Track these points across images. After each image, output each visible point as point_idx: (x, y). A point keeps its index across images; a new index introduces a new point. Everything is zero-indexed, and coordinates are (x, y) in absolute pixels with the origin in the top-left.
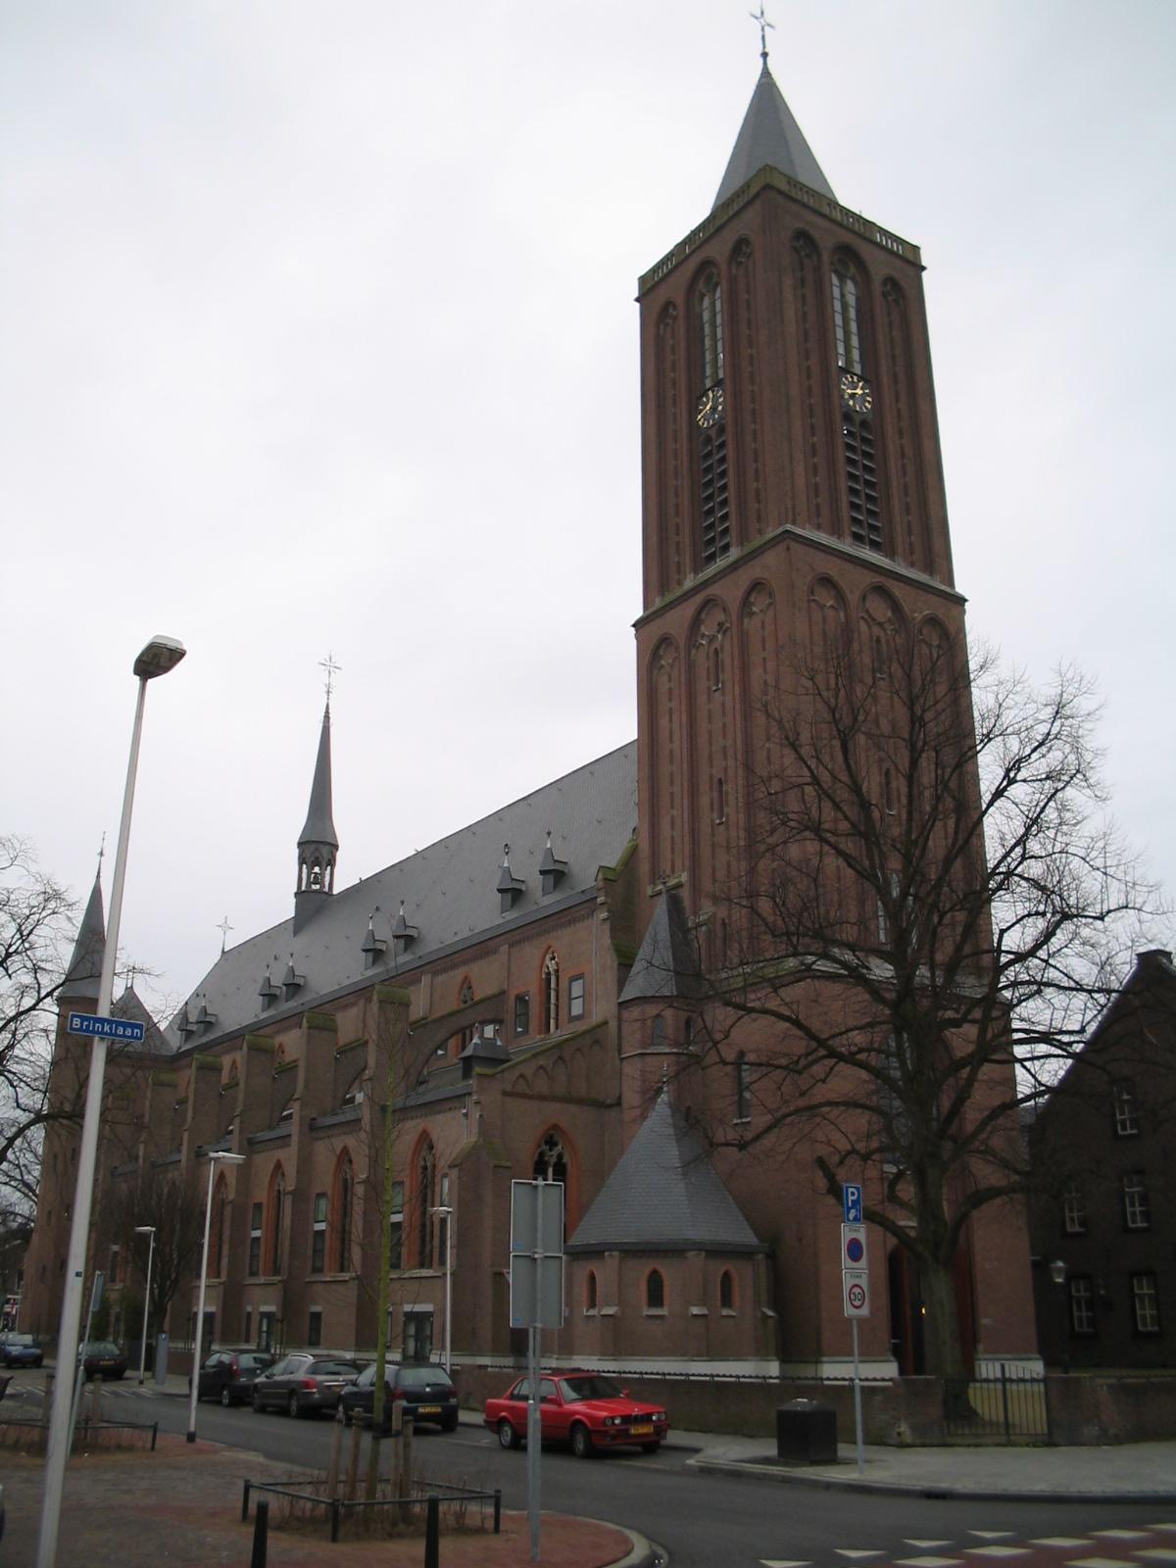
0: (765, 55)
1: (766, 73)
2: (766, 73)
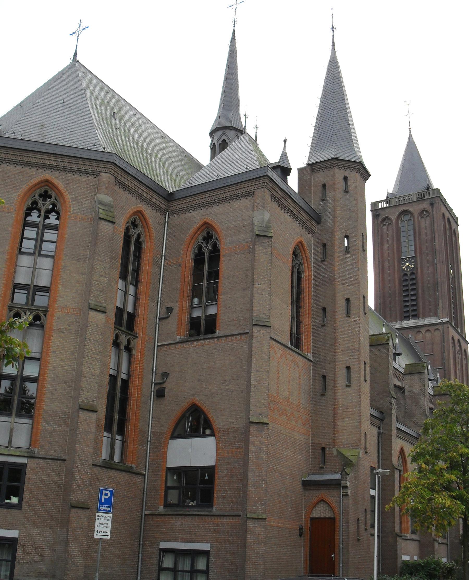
0: (410, 129)
1: (411, 137)
2: (411, 137)
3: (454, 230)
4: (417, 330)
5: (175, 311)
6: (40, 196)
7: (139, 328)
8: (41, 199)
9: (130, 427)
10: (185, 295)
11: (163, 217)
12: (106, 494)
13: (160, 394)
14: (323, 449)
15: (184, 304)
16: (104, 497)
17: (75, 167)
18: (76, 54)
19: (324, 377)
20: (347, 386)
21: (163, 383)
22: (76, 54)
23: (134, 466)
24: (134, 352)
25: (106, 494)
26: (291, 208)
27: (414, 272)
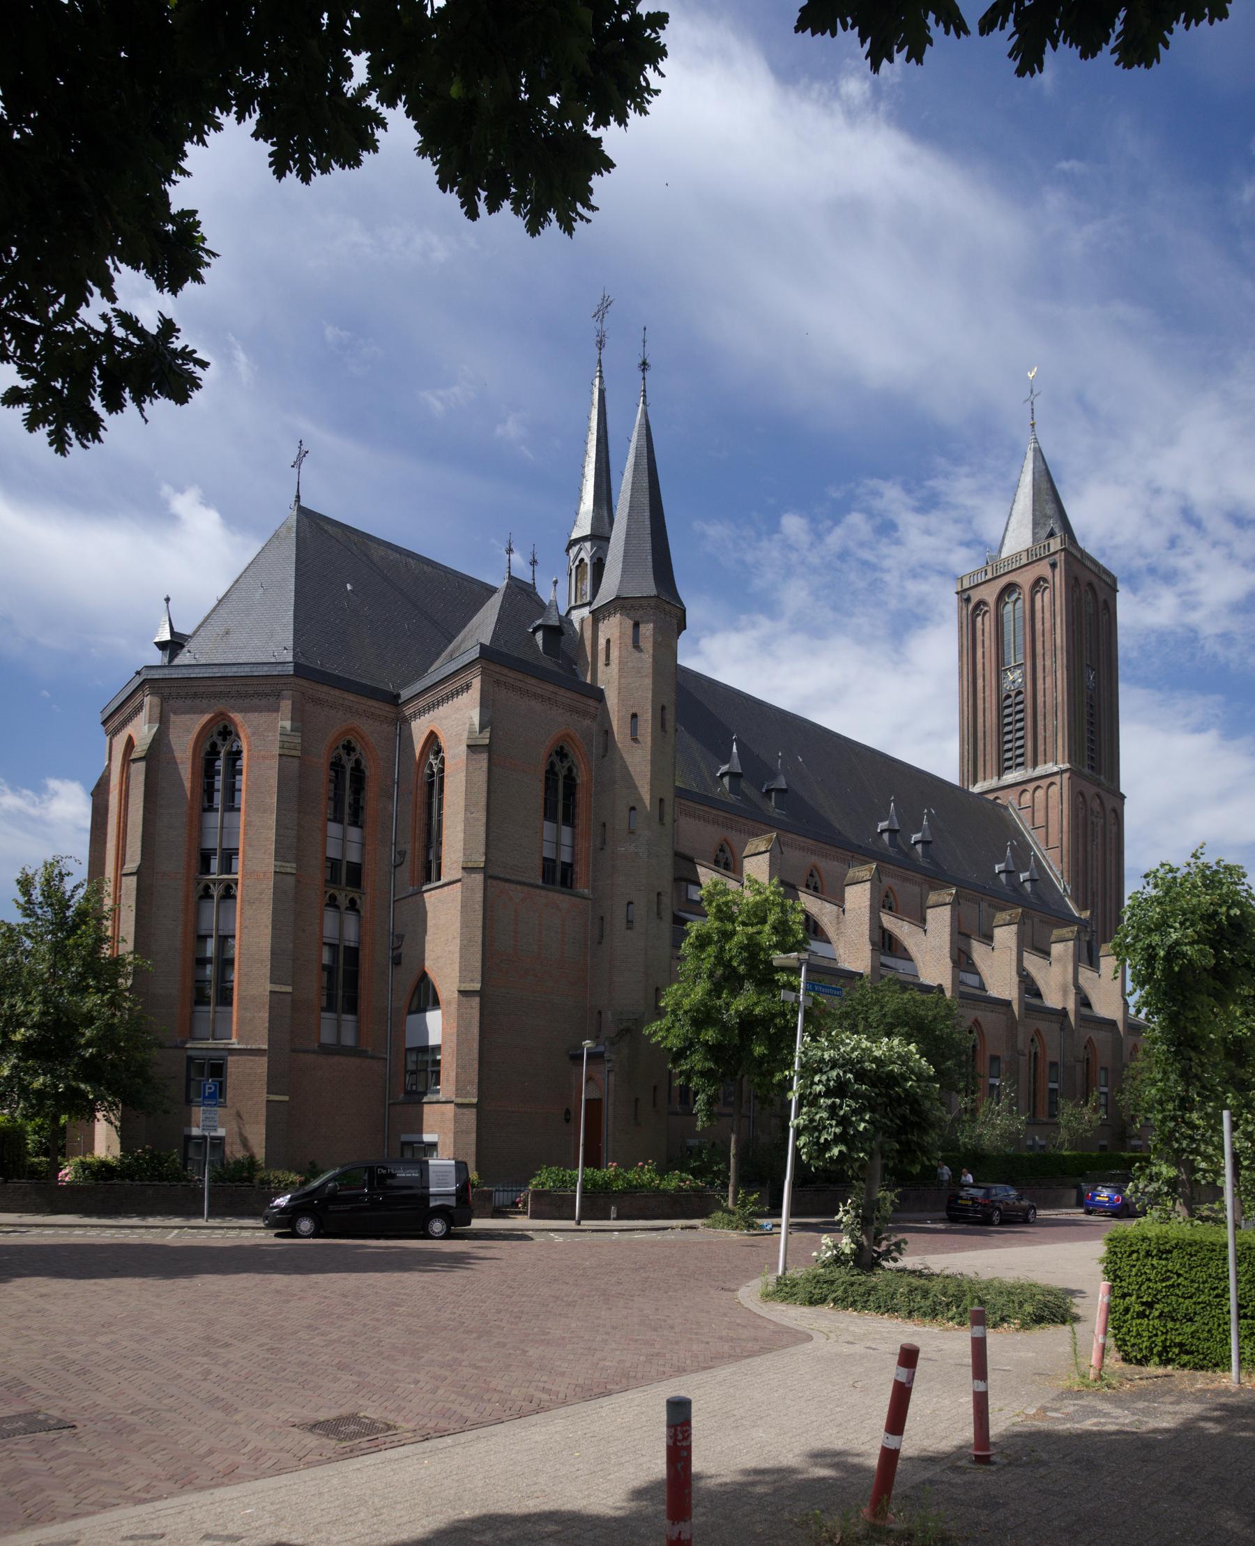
3: (1105, 602)
4: (1021, 788)
5: (408, 856)
6: (220, 734)
7: (367, 881)
8: (221, 738)
9: (362, 1004)
10: (417, 832)
11: (393, 728)
12: (210, 1088)
13: (397, 961)
14: (600, 1013)
15: (417, 844)
16: (207, 1091)
17: (251, 690)
18: (298, 497)
19: (602, 918)
20: (628, 928)
21: (399, 947)
22: (298, 497)
23: (369, 1049)
24: (362, 913)
25: (210, 1088)
26: (539, 691)
27: (1022, 690)
